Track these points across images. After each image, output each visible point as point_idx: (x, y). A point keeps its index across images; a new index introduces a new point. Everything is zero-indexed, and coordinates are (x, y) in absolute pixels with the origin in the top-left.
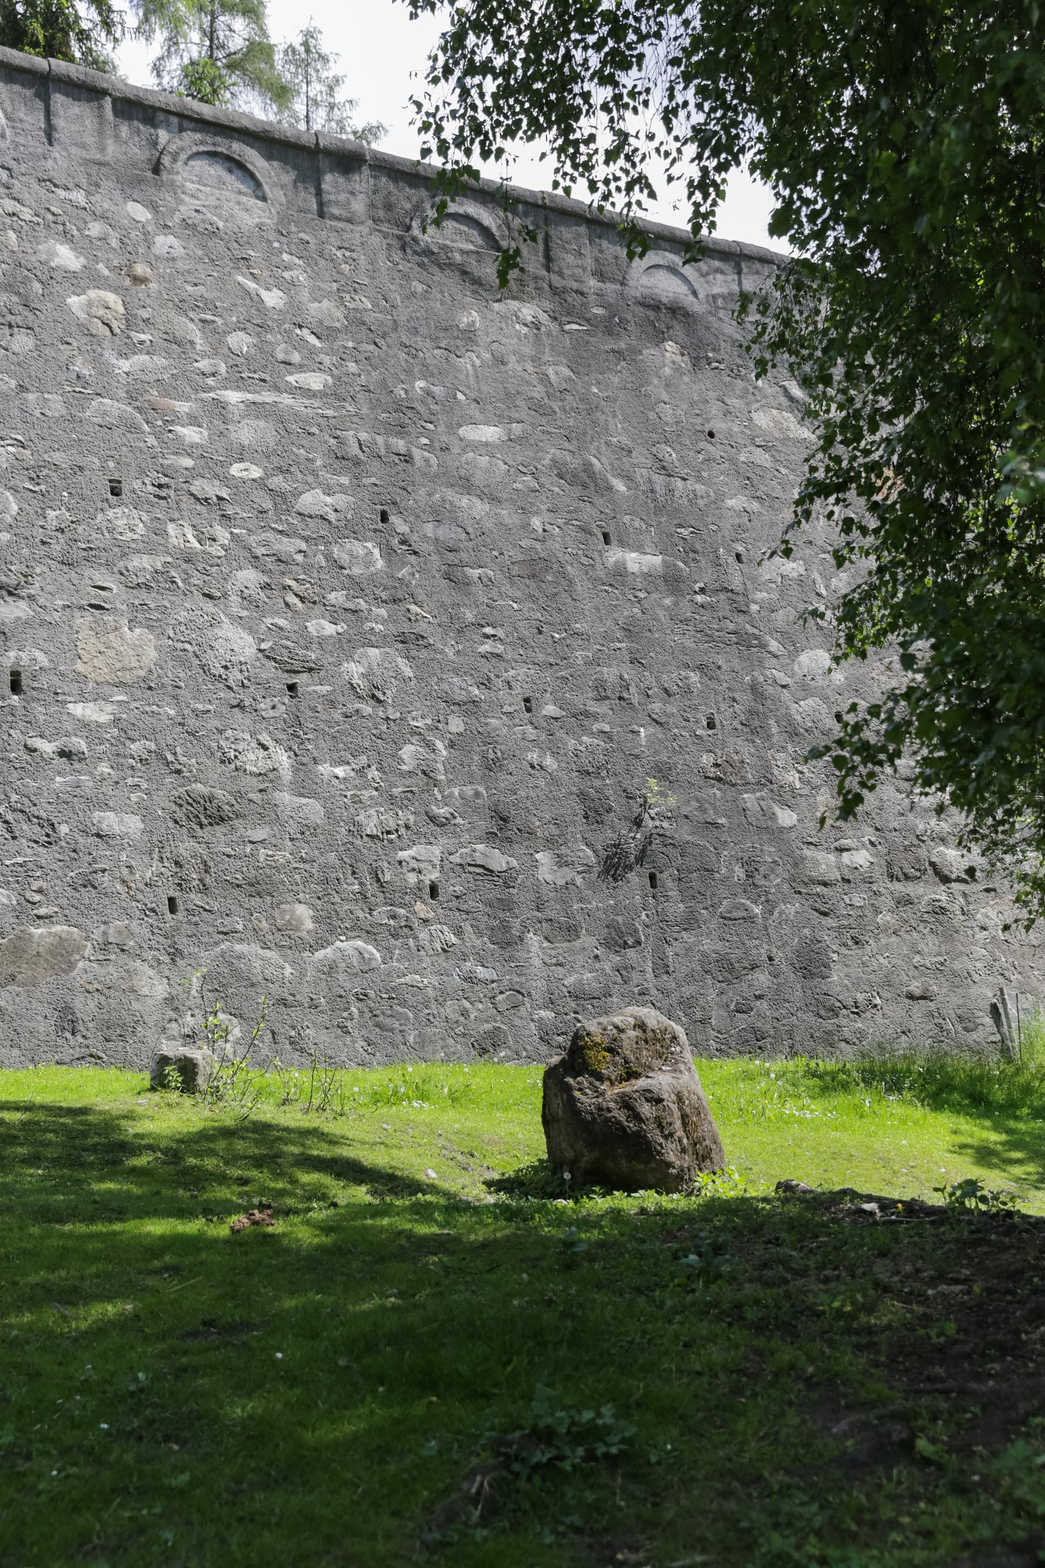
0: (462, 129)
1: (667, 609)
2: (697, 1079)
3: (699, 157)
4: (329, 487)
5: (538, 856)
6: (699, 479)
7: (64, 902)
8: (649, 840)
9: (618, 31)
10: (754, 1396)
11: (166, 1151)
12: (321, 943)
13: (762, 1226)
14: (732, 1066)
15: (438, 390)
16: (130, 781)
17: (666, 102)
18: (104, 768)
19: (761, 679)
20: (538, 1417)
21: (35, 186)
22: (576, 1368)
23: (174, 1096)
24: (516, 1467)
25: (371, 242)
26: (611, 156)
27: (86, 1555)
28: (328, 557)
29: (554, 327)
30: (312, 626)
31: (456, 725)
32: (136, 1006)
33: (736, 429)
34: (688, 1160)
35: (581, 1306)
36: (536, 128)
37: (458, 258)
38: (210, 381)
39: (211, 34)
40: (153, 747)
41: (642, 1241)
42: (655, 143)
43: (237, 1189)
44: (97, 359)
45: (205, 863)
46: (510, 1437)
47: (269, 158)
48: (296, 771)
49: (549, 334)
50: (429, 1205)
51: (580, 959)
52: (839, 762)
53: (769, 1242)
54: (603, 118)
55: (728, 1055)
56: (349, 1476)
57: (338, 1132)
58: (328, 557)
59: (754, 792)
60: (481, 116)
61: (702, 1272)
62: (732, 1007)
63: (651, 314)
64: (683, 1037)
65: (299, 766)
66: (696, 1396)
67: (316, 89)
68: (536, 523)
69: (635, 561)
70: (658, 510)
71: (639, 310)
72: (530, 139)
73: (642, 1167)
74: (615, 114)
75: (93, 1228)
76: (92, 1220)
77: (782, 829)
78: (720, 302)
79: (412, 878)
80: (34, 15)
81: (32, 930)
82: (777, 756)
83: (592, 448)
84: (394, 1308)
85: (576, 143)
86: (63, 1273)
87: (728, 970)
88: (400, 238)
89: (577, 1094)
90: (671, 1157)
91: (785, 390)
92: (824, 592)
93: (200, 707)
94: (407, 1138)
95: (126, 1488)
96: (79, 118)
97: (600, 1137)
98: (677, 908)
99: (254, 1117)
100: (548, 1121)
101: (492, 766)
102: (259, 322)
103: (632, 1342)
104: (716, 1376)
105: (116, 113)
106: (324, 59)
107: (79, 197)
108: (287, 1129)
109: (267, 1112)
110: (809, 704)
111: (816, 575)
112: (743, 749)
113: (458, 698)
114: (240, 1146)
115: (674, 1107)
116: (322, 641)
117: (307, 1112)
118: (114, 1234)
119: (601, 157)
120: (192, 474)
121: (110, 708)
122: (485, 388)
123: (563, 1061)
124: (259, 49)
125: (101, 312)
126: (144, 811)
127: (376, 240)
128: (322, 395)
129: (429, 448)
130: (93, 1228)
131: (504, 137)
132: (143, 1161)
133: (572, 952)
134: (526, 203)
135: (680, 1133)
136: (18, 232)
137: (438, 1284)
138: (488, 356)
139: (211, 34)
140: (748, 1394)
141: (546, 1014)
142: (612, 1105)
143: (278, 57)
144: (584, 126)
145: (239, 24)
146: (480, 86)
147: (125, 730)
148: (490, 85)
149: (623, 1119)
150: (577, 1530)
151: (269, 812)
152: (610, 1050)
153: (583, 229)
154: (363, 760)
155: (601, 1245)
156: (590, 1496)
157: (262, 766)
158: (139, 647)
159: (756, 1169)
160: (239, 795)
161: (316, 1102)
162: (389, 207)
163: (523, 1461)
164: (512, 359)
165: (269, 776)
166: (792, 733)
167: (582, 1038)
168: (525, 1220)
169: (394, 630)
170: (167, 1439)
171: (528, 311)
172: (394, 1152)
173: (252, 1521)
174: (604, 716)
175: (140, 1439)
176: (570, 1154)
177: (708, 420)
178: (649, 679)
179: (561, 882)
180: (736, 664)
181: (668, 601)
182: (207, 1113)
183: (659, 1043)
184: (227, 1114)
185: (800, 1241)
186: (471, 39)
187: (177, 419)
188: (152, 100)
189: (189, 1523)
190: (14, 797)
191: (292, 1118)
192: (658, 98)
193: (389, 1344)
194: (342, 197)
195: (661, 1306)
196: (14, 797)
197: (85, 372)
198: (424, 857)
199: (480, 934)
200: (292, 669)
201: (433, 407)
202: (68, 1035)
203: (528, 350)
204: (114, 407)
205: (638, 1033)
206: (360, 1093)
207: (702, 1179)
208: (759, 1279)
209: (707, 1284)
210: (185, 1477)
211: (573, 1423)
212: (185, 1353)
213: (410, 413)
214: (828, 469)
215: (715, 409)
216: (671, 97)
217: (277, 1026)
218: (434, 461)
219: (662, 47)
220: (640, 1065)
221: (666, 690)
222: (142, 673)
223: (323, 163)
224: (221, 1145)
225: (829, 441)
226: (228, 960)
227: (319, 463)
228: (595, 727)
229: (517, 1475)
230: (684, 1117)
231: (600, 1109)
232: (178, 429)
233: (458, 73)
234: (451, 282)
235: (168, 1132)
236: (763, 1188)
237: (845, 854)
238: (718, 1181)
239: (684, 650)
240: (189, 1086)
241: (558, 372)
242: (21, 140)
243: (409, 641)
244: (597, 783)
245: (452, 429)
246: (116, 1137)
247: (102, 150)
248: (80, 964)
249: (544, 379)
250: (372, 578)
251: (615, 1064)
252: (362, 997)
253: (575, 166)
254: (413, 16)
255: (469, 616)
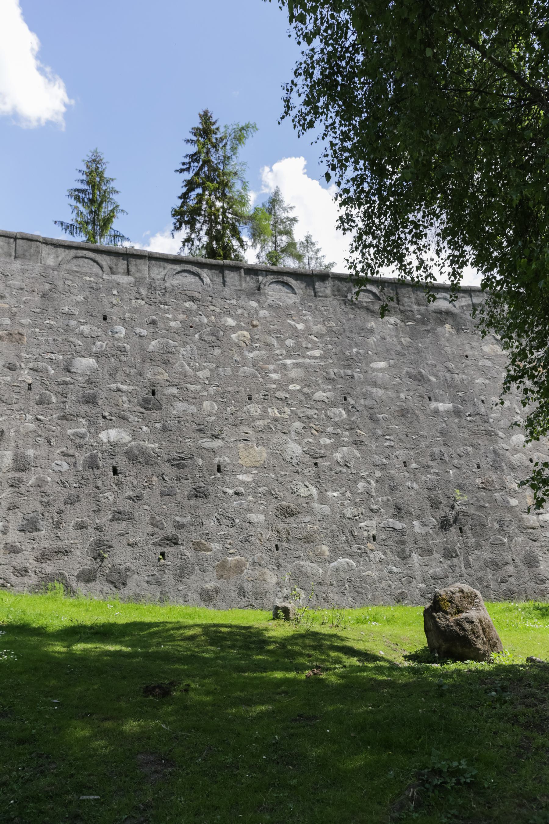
0: (363, 266)
1: (456, 423)
2: (488, 612)
3: (451, 265)
4: (324, 390)
5: (414, 523)
6: (464, 373)
7: (239, 548)
8: (458, 514)
9: (417, 226)
10: (528, 758)
11: (280, 643)
12: (332, 560)
13: (522, 678)
14: (501, 605)
15: (361, 351)
16: (259, 502)
17: (437, 248)
18: (250, 498)
19: (497, 448)
20: (434, 763)
21: (220, 300)
22: (448, 742)
23: (281, 622)
24: (427, 785)
25: (333, 303)
26: (418, 268)
27: (261, 811)
28: (326, 415)
29: (402, 324)
30: (321, 441)
31: (378, 474)
32: (266, 586)
33: (476, 353)
34: (486, 647)
35: (448, 713)
36: (390, 262)
37: (365, 304)
38: (280, 357)
39: (275, 243)
40: (267, 489)
41: (471, 684)
42: (434, 262)
43: (307, 659)
44: (242, 354)
45: (288, 531)
46: (423, 771)
47: (296, 280)
48: (319, 495)
49: (401, 327)
50: (382, 667)
51: (434, 563)
52: (533, 486)
53: (526, 686)
54: (414, 256)
55: (500, 601)
56: (359, 785)
57: (344, 635)
58: (326, 415)
59: (499, 492)
60: (370, 261)
61: (498, 700)
62: (499, 580)
63: (439, 316)
64: (479, 595)
65: (320, 493)
66: (502, 757)
67: (311, 254)
68: (402, 396)
69: (442, 406)
70: (449, 387)
71: (434, 314)
72: (388, 265)
73: (467, 650)
74: (418, 254)
75: (255, 675)
76: (254, 671)
77: (512, 507)
78: (465, 308)
79: (365, 534)
80: (220, 248)
81: (228, 558)
82: (507, 477)
83: (421, 366)
84: (371, 712)
85: (405, 266)
86: (246, 693)
87: (496, 566)
88: (343, 300)
89: (438, 620)
90: (480, 646)
91: (494, 337)
92: (519, 412)
93: (283, 473)
94: (371, 638)
95: (274, 784)
96: (233, 277)
97: (449, 639)
98: (472, 541)
99: (312, 630)
100: (427, 631)
101: (393, 489)
102: (296, 335)
103: (470, 731)
104: (509, 748)
105: (245, 273)
106: (313, 244)
107: (234, 302)
108: (324, 634)
109: (316, 628)
110: (518, 456)
111: (515, 406)
112: (493, 476)
113: (378, 464)
114: (307, 641)
115: (479, 625)
116: (325, 446)
117: (331, 627)
118: (263, 677)
119: (415, 269)
120: (276, 390)
121: (251, 476)
122: (379, 349)
123: (431, 606)
124: (292, 245)
125: (242, 338)
126: (265, 513)
127: (335, 302)
128: (320, 357)
129: (360, 372)
130: (255, 675)
131: (379, 267)
132: (272, 647)
133: (431, 560)
134: (388, 283)
135: (482, 636)
136: (215, 316)
137: (388, 702)
138: (379, 337)
139: (275, 243)
140: (525, 757)
141: (422, 586)
142: (453, 624)
143: (298, 246)
144: (407, 259)
145: (284, 238)
146: (369, 251)
147: (257, 483)
148: (372, 250)
149: (458, 630)
150: (456, 817)
151: (310, 511)
152: (450, 601)
153: (410, 289)
154: (344, 489)
155: (454, 686)
156: (460, 801)
157: (307, 494)
158: (260, 453)
159: (517, 650)
160: (299, 505)
161: (335, 623)
162: (339, 290)
163: (430, 783)
164: (388, 337)
165: (309, 497)
166: (512, 468)
167: (438, 597)
168: (421, 674)
169: (352, 440)
170: (288, 764)
171: (392, 320)
172: (366, 643)
173: (322, 802)
174: (435, 466)
175: (278, 763)
176: (437, 645)
177: (465, 351)
178: (452, 451)
179: (424, 532)
180: (486, 443)
181: (456, 421)
182: (294, 629)
183: (470, 599)
184: (302, 628)
185: (539, 686)
186: (364, 237)
187: (270, 372)
188: (257, 267)
189: (298, 801)
190: (220, 510)
191: (326, 630)
192: (433, 247)
193: (370, 728)
194: (322, 289)
195: (482, 714)
196: (220, 510)
197: (238, 359)
198: (370, 525)
199: (394, 555)
200: (315, 457)
201: (361, 358)
202: (242, 597)
203: (393, 333)
204: (248, 370)
205: (460, 594)
206: (352, 619)
207: (494, 655)
208: (524, 703)
209: (501, 705)
210: (295, 781)
211: (449, 767)
212: (292, 728)
213: (352, 361)
214: (515, 370)
215: (467, 347)
216: (438, 246)
217: (318, 593)
218: (362, 377)
219: (433, 230)
220: (463, 607)
221: (459, 455)
222: (262, 462)
223: (315, 279)
224: (300, 641)
225: (514, 361)
226: (298, 567)
227: (320, 382)
228: (432, 471)
229: (428, 789)
230: (483, 629)
231: (448, 626)
232: (270, 375)
233: (360, 248)
234: (363, 314)
235: (280, 636)
236: (521, 660)
237: (540, 516)
238: (501, 656)
239: (465, 439)
240: (287, 618)
241: (406, 340)
242: (215, 287)
243: (358, 443)
244: (435, 493)
245: (368, 364)
246: (261, 638)
247: (241, 285)
248: (245, 571)
249: (401, 343)
250: (342, 421)
251: (452, 607)
252: (349, 581)
253: (405, 273)
254: (344, 234)
255: (380, 432)
